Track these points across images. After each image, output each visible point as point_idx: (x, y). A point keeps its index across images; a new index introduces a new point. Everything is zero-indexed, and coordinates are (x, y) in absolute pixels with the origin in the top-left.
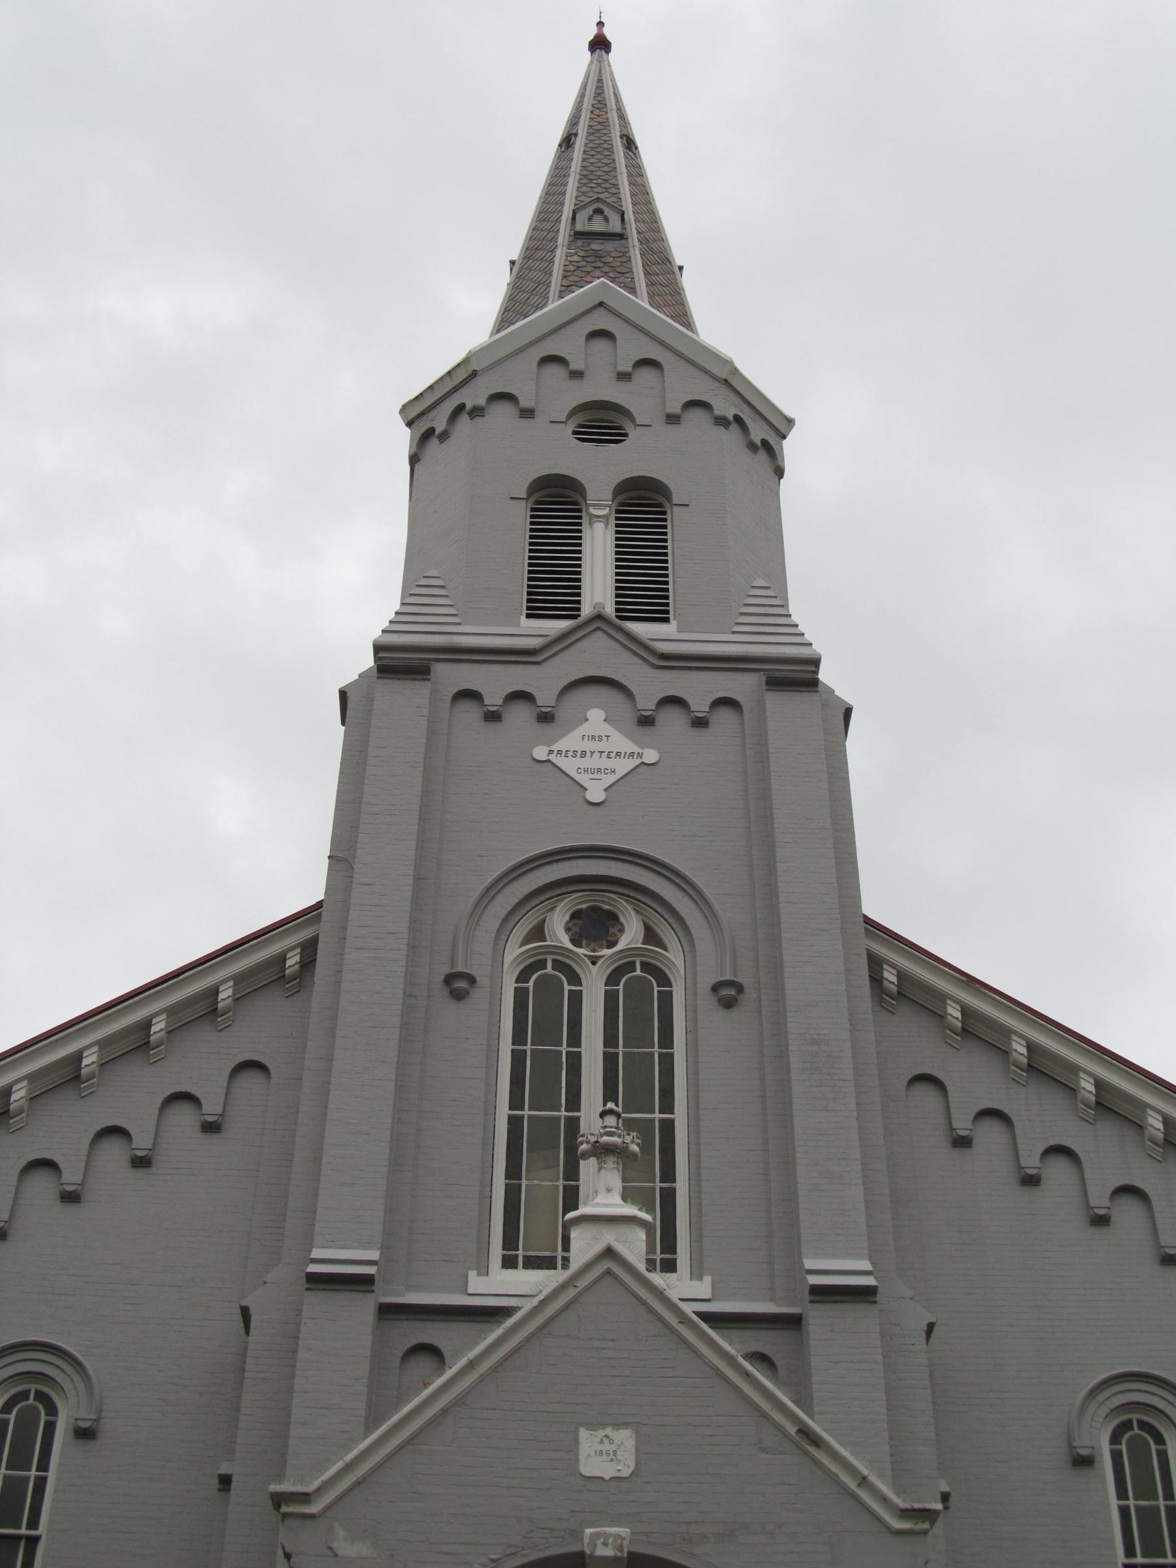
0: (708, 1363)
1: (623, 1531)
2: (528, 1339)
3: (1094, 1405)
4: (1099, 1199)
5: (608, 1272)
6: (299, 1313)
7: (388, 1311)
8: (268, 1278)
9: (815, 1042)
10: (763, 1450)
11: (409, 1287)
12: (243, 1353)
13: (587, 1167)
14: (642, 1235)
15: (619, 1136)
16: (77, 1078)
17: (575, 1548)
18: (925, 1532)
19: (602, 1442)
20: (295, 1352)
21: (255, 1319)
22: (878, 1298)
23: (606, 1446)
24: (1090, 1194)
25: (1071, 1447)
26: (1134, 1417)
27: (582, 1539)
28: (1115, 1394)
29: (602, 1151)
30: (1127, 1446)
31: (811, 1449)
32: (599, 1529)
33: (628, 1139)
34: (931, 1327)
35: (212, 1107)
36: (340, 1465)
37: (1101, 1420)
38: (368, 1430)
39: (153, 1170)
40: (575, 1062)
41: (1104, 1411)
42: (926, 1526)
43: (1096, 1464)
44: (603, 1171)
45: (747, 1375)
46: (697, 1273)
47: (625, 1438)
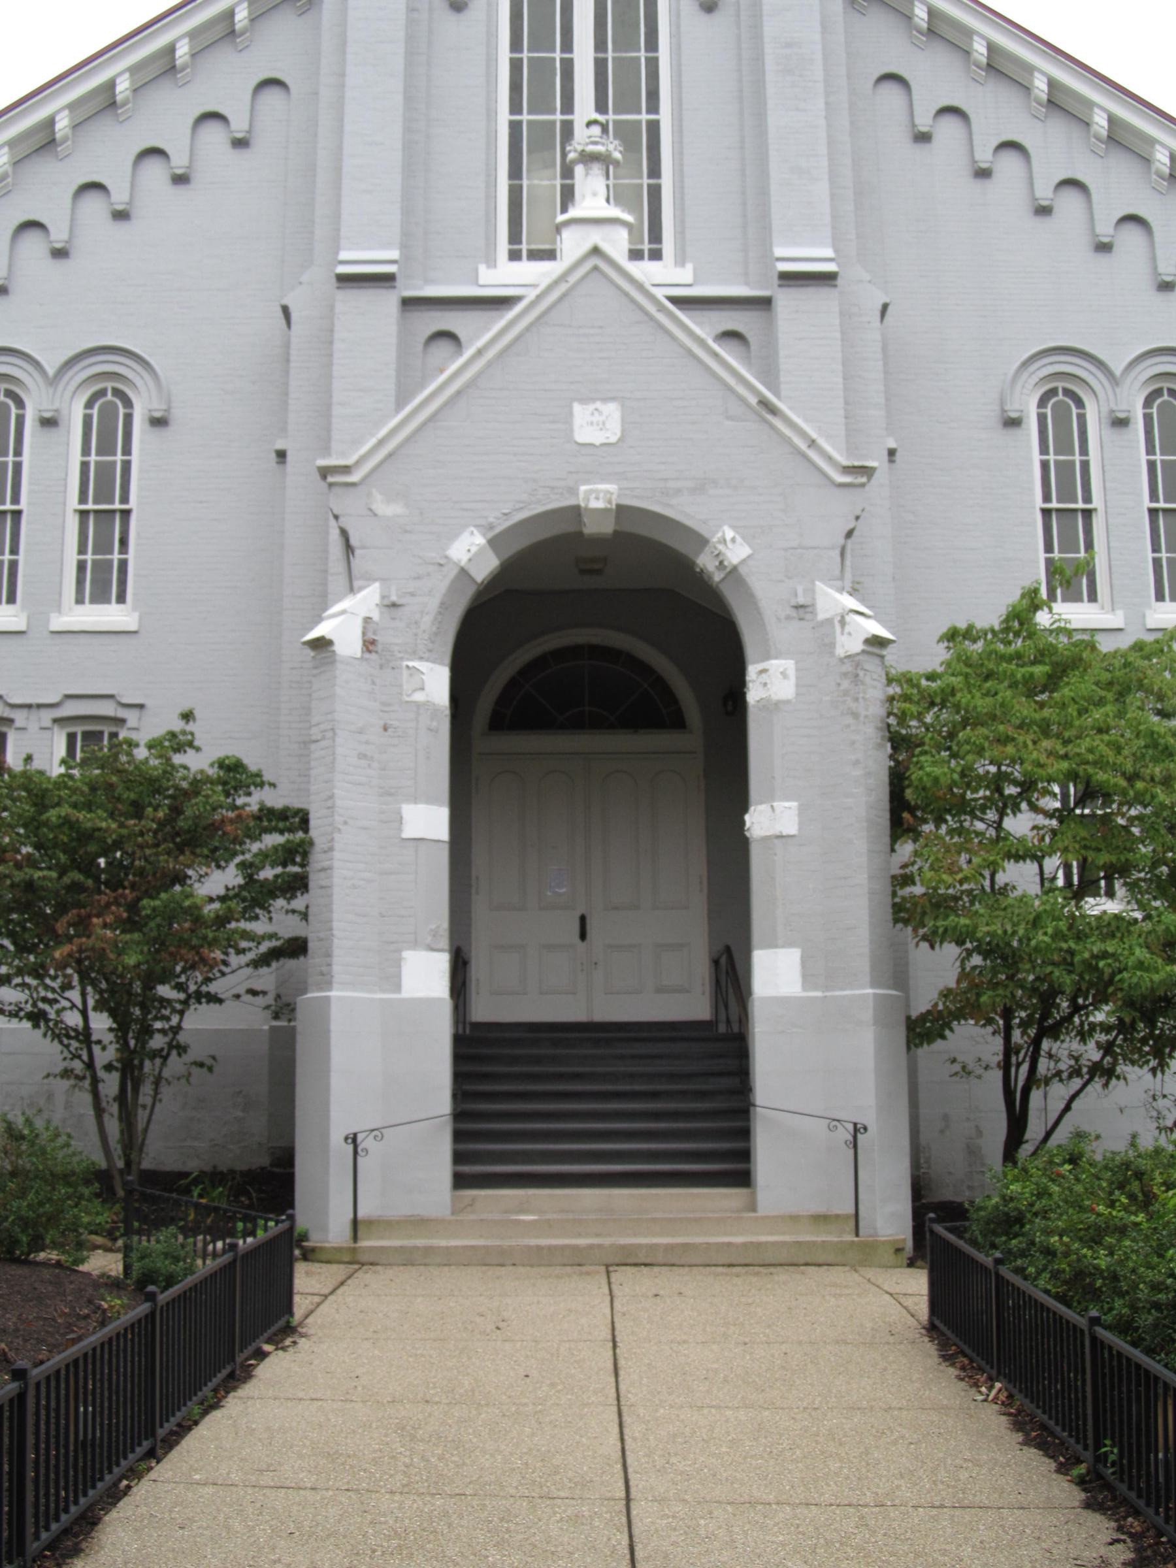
0: (682, 345)
1: (612, 487)
2: (528, 329)
3: (1025, 375)
4: (1044, 192)
5: (596, 268)
6: (332, 308)
7: (409, 303)
8: (305, 278)
9: (789, 45)
10: (729, 418)
11: (428, 281)
12: (287, 345)
13: (579, 170)
14: (623, 234)
15: (603, 144)
16: (113, 104)
17: (571, 502)
18: (863, 485)
19: (593, 414)
20: (331, 343)
21: (294, 316)
22: (839, 282)
23: (597, 418)
24: (1036, 186)
25: (1003, 411)
26: (1060, 385)
27: (577, 495)
28: (1045, 366)
29: (589, 158)
30: (1052, 409)
31: (769, 417)
32: (591, 487)
33: (611, 147)
34: (885, 307)
35: (239, 125)
36: (373, 441)
37: (1031, 387)
38: (399, 406)
39: (192, 186)
40: (568, 68)
41: (1035, 379)
42: (864, 480)
43: (1024, 425)
44: (590, 178)
45: (716, 355)
46: (681, 261)
47: (612, 411)
